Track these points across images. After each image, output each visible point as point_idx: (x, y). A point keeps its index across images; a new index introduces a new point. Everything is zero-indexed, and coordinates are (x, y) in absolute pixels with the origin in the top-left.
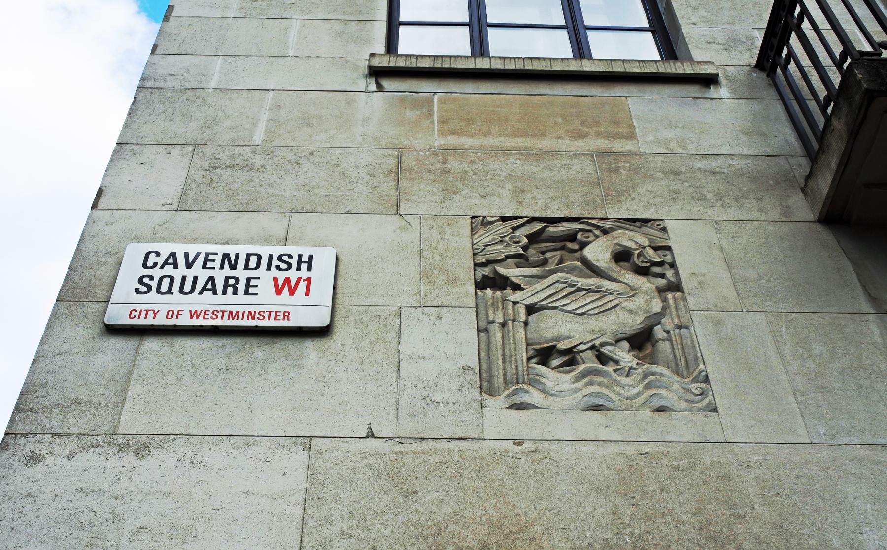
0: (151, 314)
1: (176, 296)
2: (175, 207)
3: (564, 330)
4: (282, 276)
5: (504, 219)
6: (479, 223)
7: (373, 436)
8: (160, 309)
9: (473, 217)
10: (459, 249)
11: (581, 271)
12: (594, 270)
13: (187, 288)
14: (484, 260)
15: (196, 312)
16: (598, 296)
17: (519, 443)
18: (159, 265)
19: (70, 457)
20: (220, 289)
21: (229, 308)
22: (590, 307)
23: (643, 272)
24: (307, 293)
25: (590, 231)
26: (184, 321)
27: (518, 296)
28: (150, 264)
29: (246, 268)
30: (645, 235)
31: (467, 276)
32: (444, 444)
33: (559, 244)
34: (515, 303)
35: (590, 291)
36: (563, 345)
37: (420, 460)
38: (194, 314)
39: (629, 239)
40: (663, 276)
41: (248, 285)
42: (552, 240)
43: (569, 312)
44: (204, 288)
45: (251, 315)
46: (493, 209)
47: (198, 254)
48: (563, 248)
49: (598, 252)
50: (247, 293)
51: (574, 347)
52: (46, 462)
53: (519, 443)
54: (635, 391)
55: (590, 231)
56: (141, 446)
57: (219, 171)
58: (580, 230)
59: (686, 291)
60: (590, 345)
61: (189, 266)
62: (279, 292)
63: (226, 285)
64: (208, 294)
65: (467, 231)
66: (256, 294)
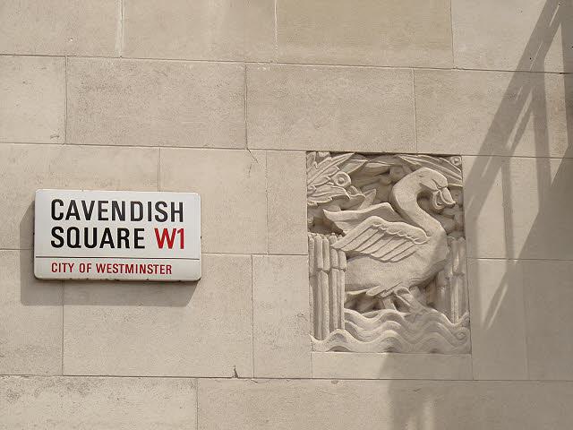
0: (68, 267)
1: (84, 250)
2: (62, 141)
3: (372, 278)
4: (161, 227)
5: (333, 154)
6: (314, 157)
7: (236, 376)
8: (77, 260)
9: (308, 152)
10: (296, 189)
11: (390, 213)
12: (399, 214)
13: (91, 242)
14: (316, 202)
15: (101, 265)
16: (402, 241)
17: (335, 381)
18: (65, 216)
19: (36, 395)
20: (116, 244)
21: (124, 262)
22: (394, 254)
23: (436, 213)
24: (181, 220)
25: (402, 167)
26: (93, 274)
27: (338, 241)
28: (57, 215)
29: (133, 219)
30: (445, 173)
31: (305, 220)
32: (283, 383)
33: (376, 178)
34: (338, 250)
35: (396, 237)
36: (370, 292)
37: (269, 397)
38: (100, 268)
39: (434, 177)
40: (453, 217)
41: (137, 238)
42: (376, 174)
43: (376, 259)
44: (103, 242)
45: (142, 268)
46: (324, 146)
47: (93, 202)
48: (378, 181)
49: (405, 193)
50: (136, 246)
51: (379, 294)
52: (22, 399)
53: (335, 381)
54: (418, 335)
55: (402, 167)
56: (81, 383)
57: (91, 93)
58: (393, 166)
59: (467, 238)
60: (389, 292)
61: (88, 217)
62: (161, 245)
63: (120, 238)
64: (107, 246)
65: (303, 169)
66: (143, 247)
